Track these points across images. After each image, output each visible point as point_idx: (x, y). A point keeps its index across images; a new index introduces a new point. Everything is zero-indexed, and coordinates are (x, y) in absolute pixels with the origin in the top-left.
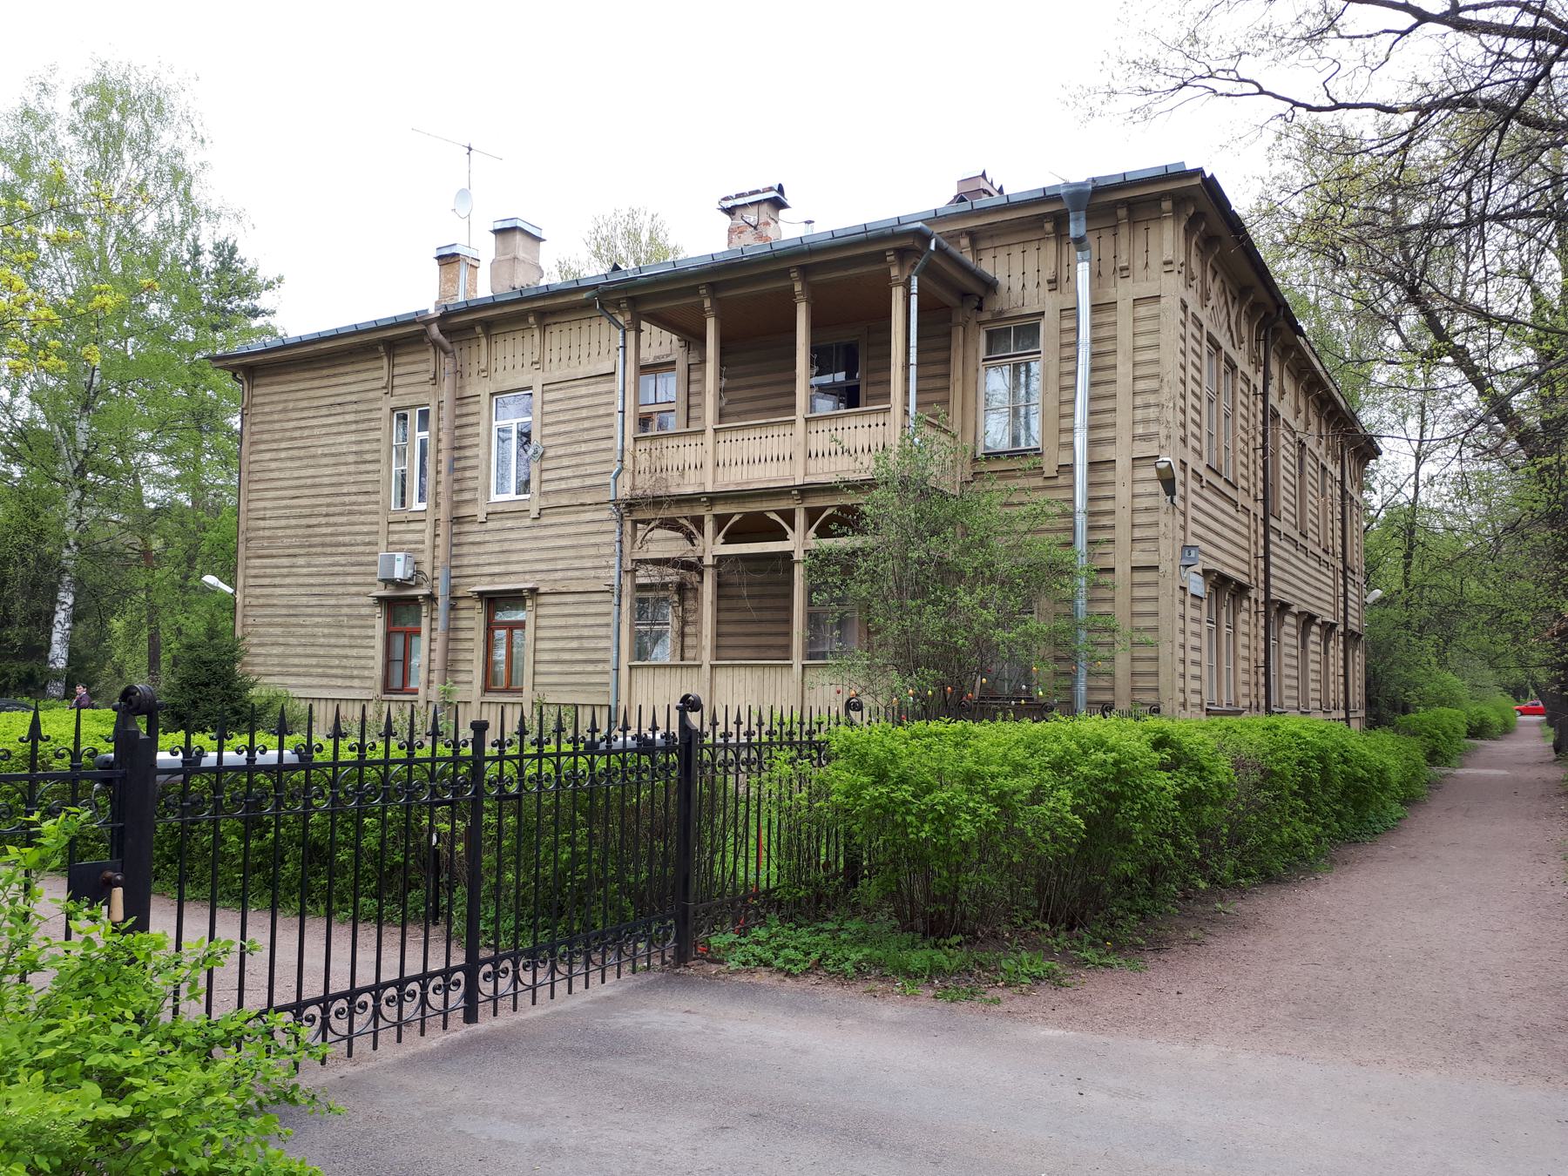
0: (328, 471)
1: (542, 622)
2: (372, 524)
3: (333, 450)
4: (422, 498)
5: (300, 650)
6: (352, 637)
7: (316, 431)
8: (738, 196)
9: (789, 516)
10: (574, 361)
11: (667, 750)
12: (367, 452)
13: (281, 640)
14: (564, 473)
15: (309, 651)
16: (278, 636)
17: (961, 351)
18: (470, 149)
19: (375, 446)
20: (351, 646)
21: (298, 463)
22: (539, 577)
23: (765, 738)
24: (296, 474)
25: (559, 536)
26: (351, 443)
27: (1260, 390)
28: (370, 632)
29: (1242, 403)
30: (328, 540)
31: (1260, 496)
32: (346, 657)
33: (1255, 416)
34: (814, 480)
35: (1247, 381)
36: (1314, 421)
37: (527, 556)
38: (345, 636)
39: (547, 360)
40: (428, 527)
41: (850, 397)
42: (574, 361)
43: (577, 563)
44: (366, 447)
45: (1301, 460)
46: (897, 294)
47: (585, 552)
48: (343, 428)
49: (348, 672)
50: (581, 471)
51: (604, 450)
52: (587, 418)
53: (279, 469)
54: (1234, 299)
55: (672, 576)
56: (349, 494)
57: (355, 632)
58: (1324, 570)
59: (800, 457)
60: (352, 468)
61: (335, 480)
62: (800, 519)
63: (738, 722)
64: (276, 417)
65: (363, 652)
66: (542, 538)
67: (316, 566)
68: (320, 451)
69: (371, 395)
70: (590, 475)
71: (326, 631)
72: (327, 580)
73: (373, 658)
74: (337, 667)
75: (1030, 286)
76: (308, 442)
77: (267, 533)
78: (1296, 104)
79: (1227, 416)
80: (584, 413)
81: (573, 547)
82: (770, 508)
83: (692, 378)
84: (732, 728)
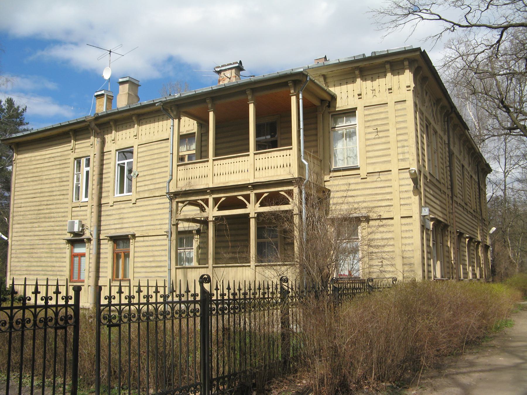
0: (48, 186)
1: (136, 249)
2: (65, 208)
3: (50, 177)
4: (86, 196)
5: (35, 264)
6: (57, 257)
7: (43, 169)
8: (222, 66)
9: (247, 197)
10: (152, 134)
11: (195, 302)
12: (64, 177)
13: (27, 259)
14: (147, 183)
15: (39, 264)
16: (25, 258)
17: (322, 124)
18: (110, 52)
19: (67, 174)
20: (56, 262)
21: (35, 183)
22: (136, 229)
23: (252, 296)
24: (34, 188)
25: (144, 211)
26: (57, 173)
27: (447, 142)
28: (64, 255)
29: (440, 148)
30: (47, 215)
31: (450, 187)
32: (54, 266)
33: (445, 153)
34: (259, 181)
35: (441, 138)
36: (467, 156)
37: (130, 220)
38: (53, 257)
39: (140, 135)
40: (88, 209)
41: (273, 145)
42: (152, 134)
43: (152, 223)
44: (64, 175)
45: (463, 172)
46: (293, 99)
47: (155, 217)
48: (54, 167)
49: (55, 273)
50: (154, 181)
51: (164, 172)
52: (157, 158)
53: (27, 186)
54: (434, 104)
55: (194, 226)
56: (56, 195)
57: (58, 255)
58: (474, 219)
59: (251, 171)
60: (57, 184)
61: (50, 190)
62: (253, 198)
63: (229, 289)
64: (27, 164)
65: (61, 264)
66: (137, 212)
67: (42, 227)
68: (44, 177)
69: (66, 153)
70: (158, 183)
71: (46, 255)
72: (46, 233)
73: (65, 267)
74: (51, 271)
75: (351, 97)
76: (40, 174)
77: (22, 213)
78: (455, 24)
79: (435, 153)
80: (156, 156)
81: (150, 215)
82: (239, 195)
83: (202, 150)
84: (226, 291)
